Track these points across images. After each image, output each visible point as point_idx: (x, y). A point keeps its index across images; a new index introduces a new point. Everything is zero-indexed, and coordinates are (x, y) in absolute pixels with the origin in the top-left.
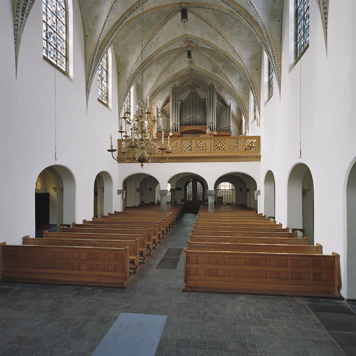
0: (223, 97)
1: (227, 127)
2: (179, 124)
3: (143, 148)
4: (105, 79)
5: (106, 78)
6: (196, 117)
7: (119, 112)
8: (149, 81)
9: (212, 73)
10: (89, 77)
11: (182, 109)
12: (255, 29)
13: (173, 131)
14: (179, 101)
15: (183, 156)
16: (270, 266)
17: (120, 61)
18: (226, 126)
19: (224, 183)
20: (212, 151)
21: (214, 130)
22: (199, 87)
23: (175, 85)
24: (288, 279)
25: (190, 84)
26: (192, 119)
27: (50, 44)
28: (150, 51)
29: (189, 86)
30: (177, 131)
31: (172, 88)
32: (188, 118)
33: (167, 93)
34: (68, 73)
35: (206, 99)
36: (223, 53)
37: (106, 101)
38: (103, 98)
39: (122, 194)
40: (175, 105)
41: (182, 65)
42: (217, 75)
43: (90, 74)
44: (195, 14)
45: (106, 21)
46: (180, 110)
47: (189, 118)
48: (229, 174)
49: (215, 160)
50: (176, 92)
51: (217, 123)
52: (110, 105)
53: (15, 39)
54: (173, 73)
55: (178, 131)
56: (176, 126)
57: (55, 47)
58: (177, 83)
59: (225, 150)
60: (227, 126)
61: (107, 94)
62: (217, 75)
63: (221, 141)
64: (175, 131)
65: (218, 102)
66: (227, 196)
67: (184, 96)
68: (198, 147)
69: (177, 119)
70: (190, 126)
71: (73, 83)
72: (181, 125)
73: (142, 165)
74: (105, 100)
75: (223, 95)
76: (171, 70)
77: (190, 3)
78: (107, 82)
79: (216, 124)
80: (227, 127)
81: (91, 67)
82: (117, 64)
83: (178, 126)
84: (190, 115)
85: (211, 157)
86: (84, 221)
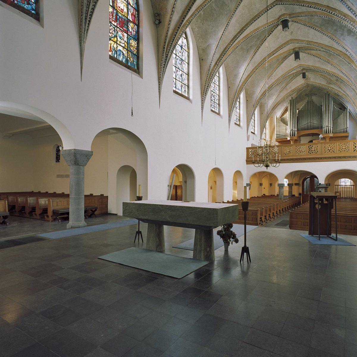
0: (341, 101)
1: (341, 130)
2: (296, 130)
3: (267, 161)
4: (238, 108)
5: (238, 107)
6: (313, 122)
7: (247, 128)
8: (270, 99)
9: (327, 85)
10: (231, 112)
11: (298, 118)
12: (352, 65)
13: (291, 136)
14: (296, 109)
15: (297, 158)
16: (341, 222)
17: (248, 92)
18: (343, 128)
19: (345, 179)
20: (323, 153)
21: (330, 133)
22: (317, 94)
23: (292, 98)
24: (352, 229)
25: (307, 93)
26: (308, 124)
27: (212, 101)
28: (272, 80)
29: (306, 95)
30: (295, 136)
31: (290, 100)
32: (304, 123)
33: (286, 104)
34: (220, 113)
35: (322, 106)
36: (333, 74)
37: (239, 122)
38: (237, 121)
39: (249, 187)
40: (293, 114)
41: (299, 82)
42: (331, 86)
43: (231, 110)
44: (314, 28)
45: (242, 77)
46: (298, 118)
47: (309, 122)
48: (336, 171)
49: (325, 160)
50: (293, 103)
51: (333, 125)
52: (241, 124)
53: (202, 107)
54: (290, 90)
55: (296, 136)
56: (294, 131)
57: (214, 101)
58: (294, 96)
59: (334, 152)
60: (344, 128)
61: (239, 117)
62: (331, 86)
63: (330, 145)
64: (293, 135)
65: (335, 107)
66: (349, 192)
67: (301, 106)
68: (310, 150)
69: (294, 125)
70: (306, 131)
71: (222, 118)
72: (298, 130)
73: (267, 169)
74: (238, 122)
75: (341, 100)
76: (288, 88)
77: (302, 47)
78: (239, 109)
79: (332, 127)
80: (343, 129)
81: (232, 106)
82: (246, 95)
83: (296, 132)
84: (308, 120)
85: (321, 158)
86: (227, 201)
